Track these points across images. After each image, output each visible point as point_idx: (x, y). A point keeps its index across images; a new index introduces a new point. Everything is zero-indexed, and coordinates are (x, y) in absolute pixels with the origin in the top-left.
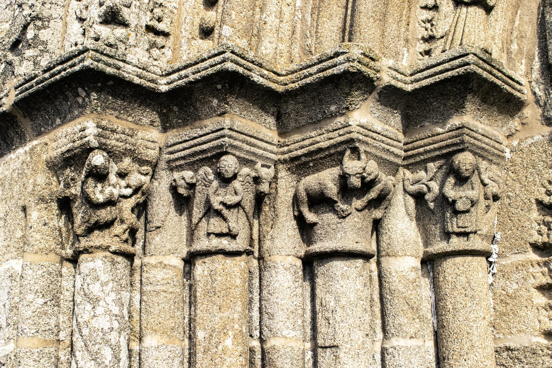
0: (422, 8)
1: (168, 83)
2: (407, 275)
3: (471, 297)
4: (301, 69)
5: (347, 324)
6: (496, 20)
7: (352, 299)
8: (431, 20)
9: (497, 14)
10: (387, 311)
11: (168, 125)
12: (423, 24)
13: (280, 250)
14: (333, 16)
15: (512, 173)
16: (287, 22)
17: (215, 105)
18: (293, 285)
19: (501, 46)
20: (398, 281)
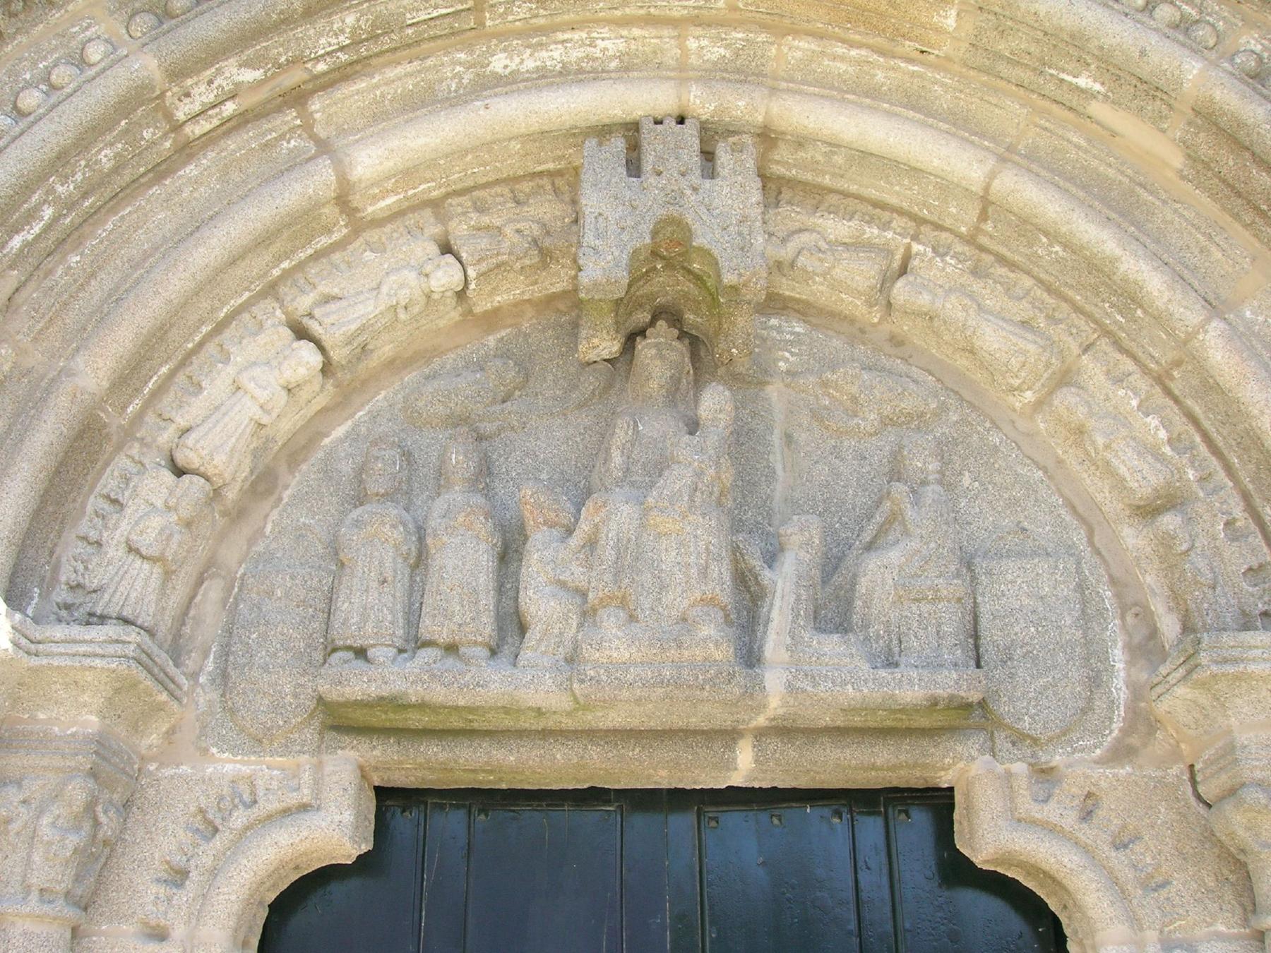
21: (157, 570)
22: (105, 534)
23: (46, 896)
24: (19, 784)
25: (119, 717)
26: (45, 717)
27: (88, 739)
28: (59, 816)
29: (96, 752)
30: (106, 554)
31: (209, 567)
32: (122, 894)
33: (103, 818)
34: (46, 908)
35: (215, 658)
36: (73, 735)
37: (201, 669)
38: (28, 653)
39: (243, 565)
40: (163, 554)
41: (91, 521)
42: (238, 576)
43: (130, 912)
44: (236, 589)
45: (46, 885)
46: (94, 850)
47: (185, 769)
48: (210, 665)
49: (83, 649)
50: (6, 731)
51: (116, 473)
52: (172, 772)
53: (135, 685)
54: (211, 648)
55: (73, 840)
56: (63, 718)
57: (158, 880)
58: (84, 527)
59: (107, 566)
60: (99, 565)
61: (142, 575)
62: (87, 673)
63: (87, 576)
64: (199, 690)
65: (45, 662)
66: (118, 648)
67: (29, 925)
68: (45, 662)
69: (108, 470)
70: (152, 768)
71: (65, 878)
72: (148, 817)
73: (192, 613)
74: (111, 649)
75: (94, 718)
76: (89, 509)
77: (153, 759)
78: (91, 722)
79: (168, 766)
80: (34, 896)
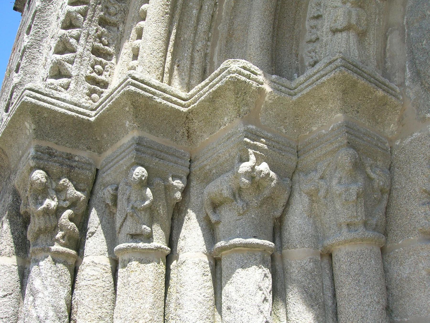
0: (307, 42)
1: (96, 114)
2: (305, 265)
3: (365, 283)
4: (199, 90)
5: (246, 312)
6: (369, 44)
7: (251, 289)
8: (315, 50)
9: (370, 39)
10: (288, 300)
11: (102, 150)
12: (309, 54)
13: (191, 247)
14: (235, 56)
15: (398, 168)
16: (197, 63)
17: (128, 126)
18: (201, 278)
19: (376, 64)
20: (297, 271)
21: (352, 35)
22: (319, 33)
23: (352, 228)
24: (316, 170)
25: (358, 112)
26: (316, 128)
27: (339, 127)
28: (341, 178)
29: (347, 132)
30: (322, 40)
31: (388, 29)
32: (404, 219)
33: (373, 175)
34: (353, 235)
35: (409, 69)
36: (332, 129)
37: (404, 79)
38: (290, 95)
39: (405, 17)
40: (349, 23)
41: (311, 32)
42: (405, 24)
43: (412, 228)
44: (406, 30)
45: (349, 221)
46: (375, 196)
47: (416, 134)
48: (408, 74)
49: (314, 78)
50: (301, 146)
51: (313, 5)
52: (409, 140)
53: (354, 84)
54: (405, 66)
55: (354, 189)
56: (325, 124)
57: (424, 204)
58: (308, 37)
59: (325, 46)
60: (321, 47)
61: (344, 39)
62: (323, 89)
63: (317, 56)
64: (408, 90)
65: (299, 95)
66: (333, 66)
67: (348, 248)
68: (299, 95)
69: (309, 7)
70: (397, 144)
71: (359, 214)
72: (404, 171)
73: (388, 55)
74: (329, 68)
75: (339, 115)
76: (307, 27)
77: (396, 139)
78: (339, 117)
79: (406, 138)
80: (345, 229)
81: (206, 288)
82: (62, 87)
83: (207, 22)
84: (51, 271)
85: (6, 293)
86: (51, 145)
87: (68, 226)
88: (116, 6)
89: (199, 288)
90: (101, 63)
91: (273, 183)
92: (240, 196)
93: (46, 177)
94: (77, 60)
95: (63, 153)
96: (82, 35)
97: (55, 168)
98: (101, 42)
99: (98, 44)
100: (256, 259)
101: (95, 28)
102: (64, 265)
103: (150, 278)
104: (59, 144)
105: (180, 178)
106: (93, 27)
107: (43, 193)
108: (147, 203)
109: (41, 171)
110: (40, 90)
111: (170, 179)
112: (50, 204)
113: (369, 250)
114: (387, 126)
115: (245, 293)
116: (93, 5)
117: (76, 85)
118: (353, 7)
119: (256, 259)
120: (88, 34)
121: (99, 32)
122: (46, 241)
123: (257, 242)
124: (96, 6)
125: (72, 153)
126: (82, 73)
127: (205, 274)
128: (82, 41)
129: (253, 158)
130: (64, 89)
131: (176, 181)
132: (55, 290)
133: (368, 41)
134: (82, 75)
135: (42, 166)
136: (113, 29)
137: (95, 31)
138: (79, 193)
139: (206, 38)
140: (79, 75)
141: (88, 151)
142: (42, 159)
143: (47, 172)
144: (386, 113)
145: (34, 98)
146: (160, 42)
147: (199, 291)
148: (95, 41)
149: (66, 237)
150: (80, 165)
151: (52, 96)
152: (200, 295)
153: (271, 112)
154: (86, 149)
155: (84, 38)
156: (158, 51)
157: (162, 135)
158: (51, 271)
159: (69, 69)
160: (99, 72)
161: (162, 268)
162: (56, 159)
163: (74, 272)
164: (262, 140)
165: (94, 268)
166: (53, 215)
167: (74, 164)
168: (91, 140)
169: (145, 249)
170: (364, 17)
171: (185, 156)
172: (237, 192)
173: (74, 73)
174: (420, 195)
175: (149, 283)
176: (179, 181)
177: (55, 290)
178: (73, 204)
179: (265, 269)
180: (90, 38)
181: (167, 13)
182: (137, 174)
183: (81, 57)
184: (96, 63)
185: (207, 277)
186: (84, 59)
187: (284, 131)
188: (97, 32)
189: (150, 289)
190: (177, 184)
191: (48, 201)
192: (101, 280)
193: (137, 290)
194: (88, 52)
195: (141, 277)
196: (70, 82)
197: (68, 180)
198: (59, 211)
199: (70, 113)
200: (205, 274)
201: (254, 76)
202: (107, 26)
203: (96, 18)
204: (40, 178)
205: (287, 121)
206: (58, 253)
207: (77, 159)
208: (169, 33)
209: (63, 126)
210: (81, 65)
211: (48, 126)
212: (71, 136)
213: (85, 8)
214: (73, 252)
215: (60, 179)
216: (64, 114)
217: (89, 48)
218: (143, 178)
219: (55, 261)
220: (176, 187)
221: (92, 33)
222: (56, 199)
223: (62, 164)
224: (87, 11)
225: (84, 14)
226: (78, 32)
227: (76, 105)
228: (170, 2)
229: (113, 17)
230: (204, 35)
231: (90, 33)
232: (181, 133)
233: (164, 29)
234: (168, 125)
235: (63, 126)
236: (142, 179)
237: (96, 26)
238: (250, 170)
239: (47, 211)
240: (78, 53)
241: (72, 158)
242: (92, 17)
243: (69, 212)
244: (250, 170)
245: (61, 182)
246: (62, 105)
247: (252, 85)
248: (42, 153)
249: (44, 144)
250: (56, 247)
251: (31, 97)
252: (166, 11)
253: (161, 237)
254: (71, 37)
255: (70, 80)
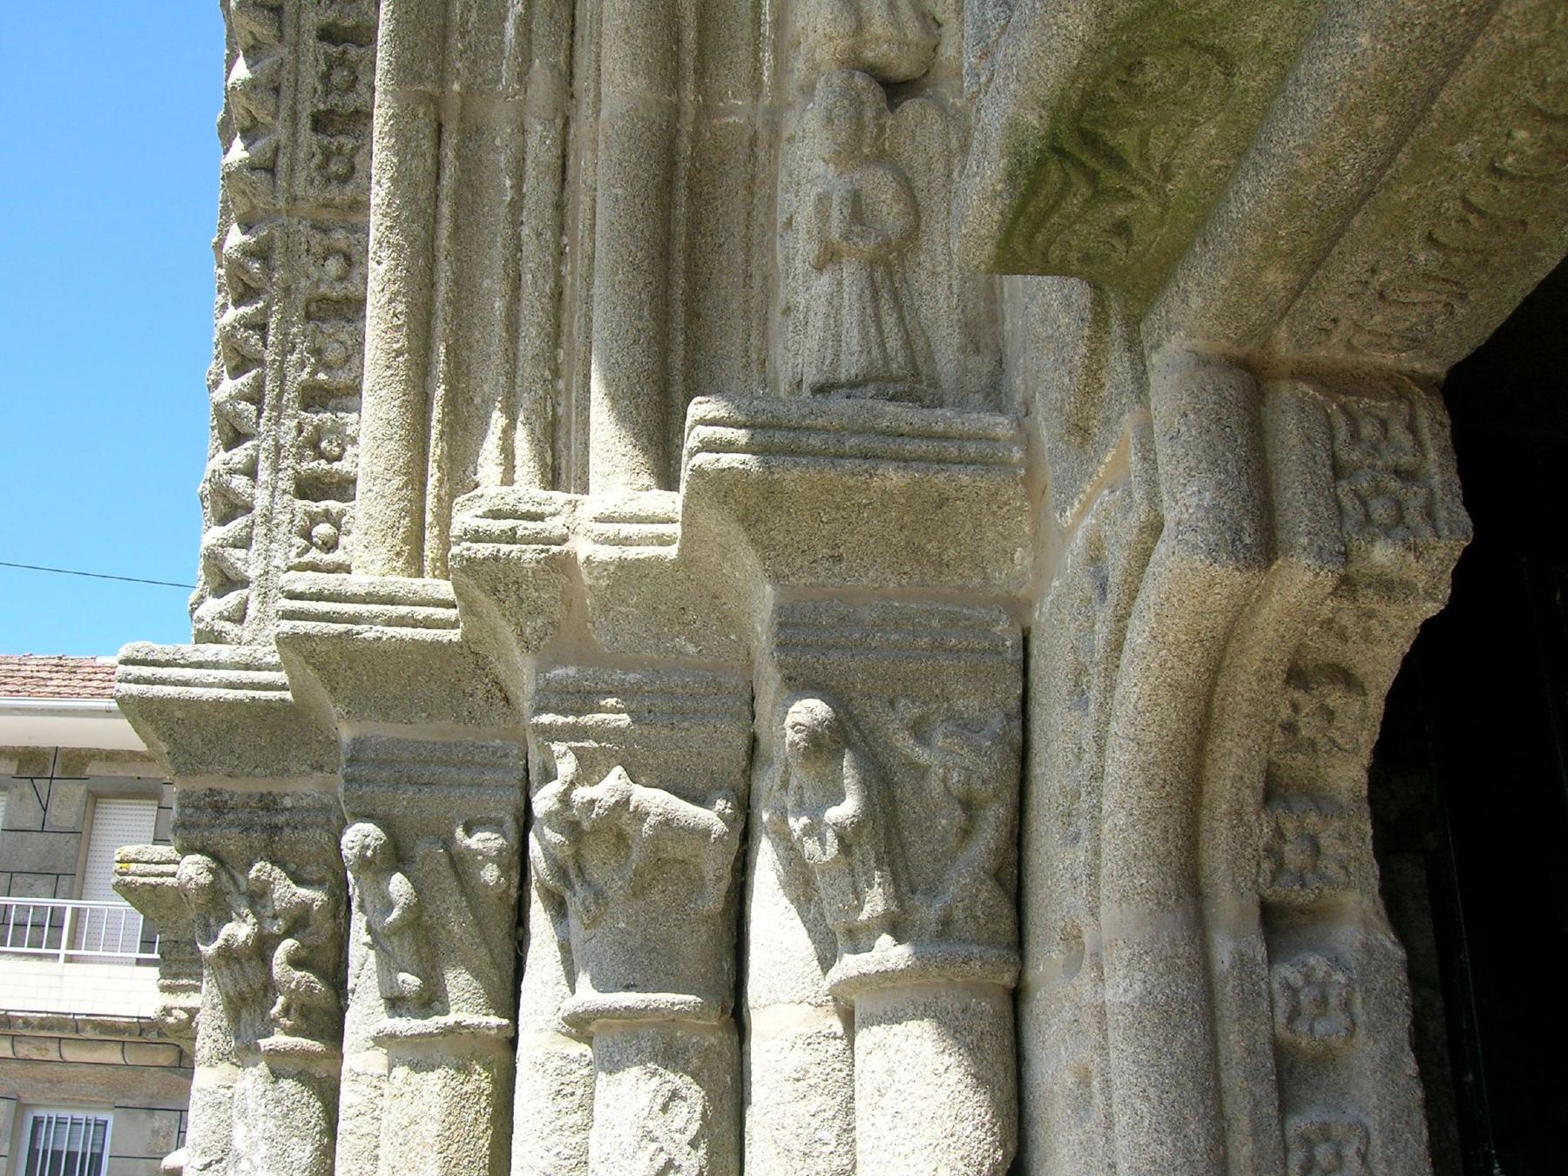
81: (567, 1133)
82: (228, 619)
83: (539, 324)
84: (264, 1101)
85: (207, 1160)
86: (215, 782)
87: (290, 982)
88: (343, 337)
89: (544, 1135)
90: (327, 516)
91: (646, 826)
92: (581, 870)
93: (210, 870)
94: (259, 531)
95: (249, 796)
96: (262, 457)
97: (231, 841)
98: (320, 455)
99: (311, 465)
100: (640, 1051)
101: (294, 423)
102: (299, 1081)
103: (434, 1111)
104: (236, 776)
105: (497, 826)
106: (287, 422)
107: (214, 908)
108: (396, 913)
109: (197, 857)
110: (150, 658)
111: (459, 833)
112: (234, 936)
113: (922, 1008)
114: (997, 561)
115: (611, 1151)
116: (274, 360)
117: (263, 603)
118: (842, 173)
119: (640, 1051)
120: (278, 448)
121: (308, 429)
122: (252, 1026)
123: (624, 1004)
124: (282, 362)
125: (275, 791)
126: (276, 562)
127: (564, 1092)
128: (264, 475)
129: (566, 767)
130: (234, 621)
131: (479, 835)
132: (274, 1151)
133: (928, 265)
134: (277, 567)
135: (198, 844)
136: (350, 404)
137: (294, 433)
138: (304, 893)
139: (542, 375)
140: (267, 573)
141: (317, 774)
142: (195, 825)
143: (214, 856)
144: (968, 526)
145: (137, 681)
146: (392, 445)
147: (541, 1143)
148: (300, 458)
149: (292, 1011)
150: (298, 818)
151: (182, 662)
152: (545, 1154)
153: (622, 609)
154: (308, 769)
155: (267, 464)
156: (388, 477)
157: (424, 715)
158: (264, 1101)
159: (239, 564)
160: (324, 543)
161: (481, 1080)
162: (231, 816)
163: (328, 1094)
164: (611, 701)
165: (354, 1088)
166: (251, 959)
167: (281, 819)
168: (316, 746)
169: (413, 1035)
170: (885, 193)
171: (506, 756)
172: (571, 863)
173: (252, 573)
174: (1066, 805)
175: (429, 1127)
176: (487, 835)
177: (274, 1151)
178: (298, 922)
179: (670, 1076)
180: (285, 457)
181: (399, 353)
182: (350, 845)
183: (268, 518)
184: (314, 519)
185: (571, 1098)
186: (275, 522)
187: (691, 649)
188: (300, 432)
189: (432, 1141)
190: (480, 846)
191: (227, 930)
192: (368, 1117)
193: (403, 1148)
194: (288, 497)
195: (414, 1110)
196: (247, 599)
197: (269, 866)
198: (263, 947)
199: (232, 694)
200: (564, 1092)
201: (530, 525)
202: (332, 403)
203: (291, 394)
204: (194, 876)
205: (691, 615)
206: (274, 1053)
207: (288, 802)
208: (425, 401)
209: (232, 729)
210: (271, 542)
211: (196, 739)
212: (262, 748)
213: (255, 378)
214: (317, 1046)
215: (250, 866)
216: (217, 703)
217: (286, 484)
218: (369, 853)
219: (276, 1075)
220: (477, 852)
221: (288, 440)
222: (251, 919)
223: (247, 828)
224: (264, 382)
225: (255, 396)
226: (250, 452)
227: (247, 667)
228: (402, 318)
229: (340, 372)
230: (535, 367)
231: (282, 442)
232: (480, 694)
233: (397, 403)
234: (432, 685)
235: (232, 729)
236: (365, 856)
237: (295, 416)
238: (557, 806)
239: (228, 954)
240: (257, 511)
241: (275, 803)
242: (279, 397)
243: (288, 944)
244: (557, 806)
245: (253, 874)
246: (211, 680)
247: (520, 558)
248: (197, 808)
249: (200, 784)
250: (280, 1040)
251: (130, 682)
252: (396, 346)
253: (467, 996)
254: (232, 472)
255: (246, 591)
